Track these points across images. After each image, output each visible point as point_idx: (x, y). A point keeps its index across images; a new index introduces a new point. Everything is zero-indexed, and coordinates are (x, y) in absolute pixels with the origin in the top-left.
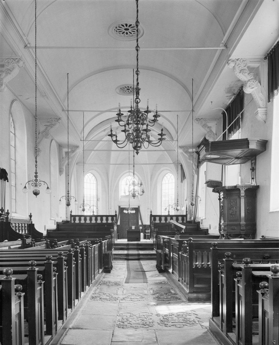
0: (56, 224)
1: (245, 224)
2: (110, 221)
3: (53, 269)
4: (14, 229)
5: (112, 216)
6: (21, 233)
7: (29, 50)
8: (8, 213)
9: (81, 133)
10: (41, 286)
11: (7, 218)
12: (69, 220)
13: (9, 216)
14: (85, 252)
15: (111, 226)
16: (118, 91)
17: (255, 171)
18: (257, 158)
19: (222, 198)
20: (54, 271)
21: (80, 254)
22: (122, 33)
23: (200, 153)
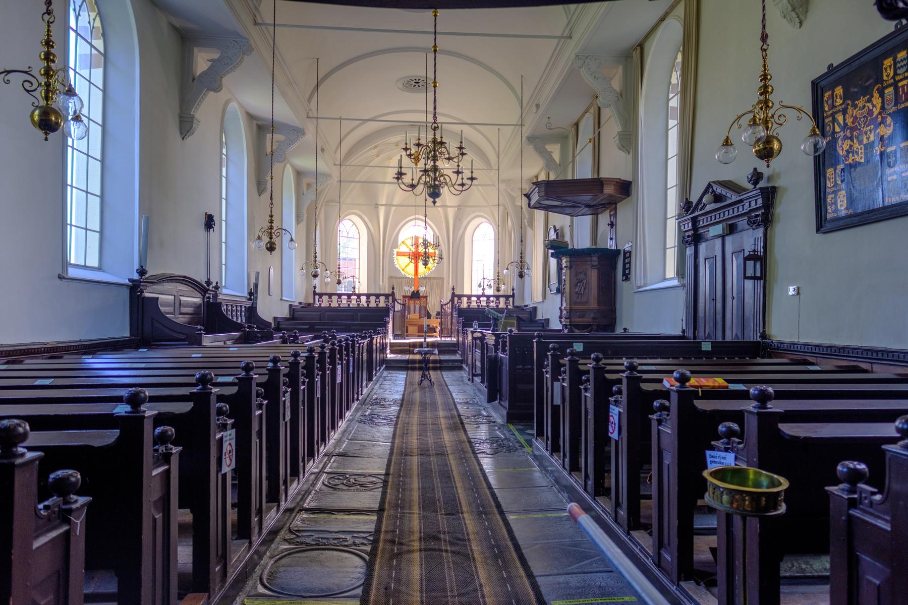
0: (886, 490)
2: (382, 304)
3: (283, 380)
5: (387, 296)
6: (239, 321)
8: (217, 288)
10: (262, 409)
12: (311, 301)
15: (386, 311)
16: (400, 86)
17: (614, 227)
20: (302, 375)
21: (328, 358)
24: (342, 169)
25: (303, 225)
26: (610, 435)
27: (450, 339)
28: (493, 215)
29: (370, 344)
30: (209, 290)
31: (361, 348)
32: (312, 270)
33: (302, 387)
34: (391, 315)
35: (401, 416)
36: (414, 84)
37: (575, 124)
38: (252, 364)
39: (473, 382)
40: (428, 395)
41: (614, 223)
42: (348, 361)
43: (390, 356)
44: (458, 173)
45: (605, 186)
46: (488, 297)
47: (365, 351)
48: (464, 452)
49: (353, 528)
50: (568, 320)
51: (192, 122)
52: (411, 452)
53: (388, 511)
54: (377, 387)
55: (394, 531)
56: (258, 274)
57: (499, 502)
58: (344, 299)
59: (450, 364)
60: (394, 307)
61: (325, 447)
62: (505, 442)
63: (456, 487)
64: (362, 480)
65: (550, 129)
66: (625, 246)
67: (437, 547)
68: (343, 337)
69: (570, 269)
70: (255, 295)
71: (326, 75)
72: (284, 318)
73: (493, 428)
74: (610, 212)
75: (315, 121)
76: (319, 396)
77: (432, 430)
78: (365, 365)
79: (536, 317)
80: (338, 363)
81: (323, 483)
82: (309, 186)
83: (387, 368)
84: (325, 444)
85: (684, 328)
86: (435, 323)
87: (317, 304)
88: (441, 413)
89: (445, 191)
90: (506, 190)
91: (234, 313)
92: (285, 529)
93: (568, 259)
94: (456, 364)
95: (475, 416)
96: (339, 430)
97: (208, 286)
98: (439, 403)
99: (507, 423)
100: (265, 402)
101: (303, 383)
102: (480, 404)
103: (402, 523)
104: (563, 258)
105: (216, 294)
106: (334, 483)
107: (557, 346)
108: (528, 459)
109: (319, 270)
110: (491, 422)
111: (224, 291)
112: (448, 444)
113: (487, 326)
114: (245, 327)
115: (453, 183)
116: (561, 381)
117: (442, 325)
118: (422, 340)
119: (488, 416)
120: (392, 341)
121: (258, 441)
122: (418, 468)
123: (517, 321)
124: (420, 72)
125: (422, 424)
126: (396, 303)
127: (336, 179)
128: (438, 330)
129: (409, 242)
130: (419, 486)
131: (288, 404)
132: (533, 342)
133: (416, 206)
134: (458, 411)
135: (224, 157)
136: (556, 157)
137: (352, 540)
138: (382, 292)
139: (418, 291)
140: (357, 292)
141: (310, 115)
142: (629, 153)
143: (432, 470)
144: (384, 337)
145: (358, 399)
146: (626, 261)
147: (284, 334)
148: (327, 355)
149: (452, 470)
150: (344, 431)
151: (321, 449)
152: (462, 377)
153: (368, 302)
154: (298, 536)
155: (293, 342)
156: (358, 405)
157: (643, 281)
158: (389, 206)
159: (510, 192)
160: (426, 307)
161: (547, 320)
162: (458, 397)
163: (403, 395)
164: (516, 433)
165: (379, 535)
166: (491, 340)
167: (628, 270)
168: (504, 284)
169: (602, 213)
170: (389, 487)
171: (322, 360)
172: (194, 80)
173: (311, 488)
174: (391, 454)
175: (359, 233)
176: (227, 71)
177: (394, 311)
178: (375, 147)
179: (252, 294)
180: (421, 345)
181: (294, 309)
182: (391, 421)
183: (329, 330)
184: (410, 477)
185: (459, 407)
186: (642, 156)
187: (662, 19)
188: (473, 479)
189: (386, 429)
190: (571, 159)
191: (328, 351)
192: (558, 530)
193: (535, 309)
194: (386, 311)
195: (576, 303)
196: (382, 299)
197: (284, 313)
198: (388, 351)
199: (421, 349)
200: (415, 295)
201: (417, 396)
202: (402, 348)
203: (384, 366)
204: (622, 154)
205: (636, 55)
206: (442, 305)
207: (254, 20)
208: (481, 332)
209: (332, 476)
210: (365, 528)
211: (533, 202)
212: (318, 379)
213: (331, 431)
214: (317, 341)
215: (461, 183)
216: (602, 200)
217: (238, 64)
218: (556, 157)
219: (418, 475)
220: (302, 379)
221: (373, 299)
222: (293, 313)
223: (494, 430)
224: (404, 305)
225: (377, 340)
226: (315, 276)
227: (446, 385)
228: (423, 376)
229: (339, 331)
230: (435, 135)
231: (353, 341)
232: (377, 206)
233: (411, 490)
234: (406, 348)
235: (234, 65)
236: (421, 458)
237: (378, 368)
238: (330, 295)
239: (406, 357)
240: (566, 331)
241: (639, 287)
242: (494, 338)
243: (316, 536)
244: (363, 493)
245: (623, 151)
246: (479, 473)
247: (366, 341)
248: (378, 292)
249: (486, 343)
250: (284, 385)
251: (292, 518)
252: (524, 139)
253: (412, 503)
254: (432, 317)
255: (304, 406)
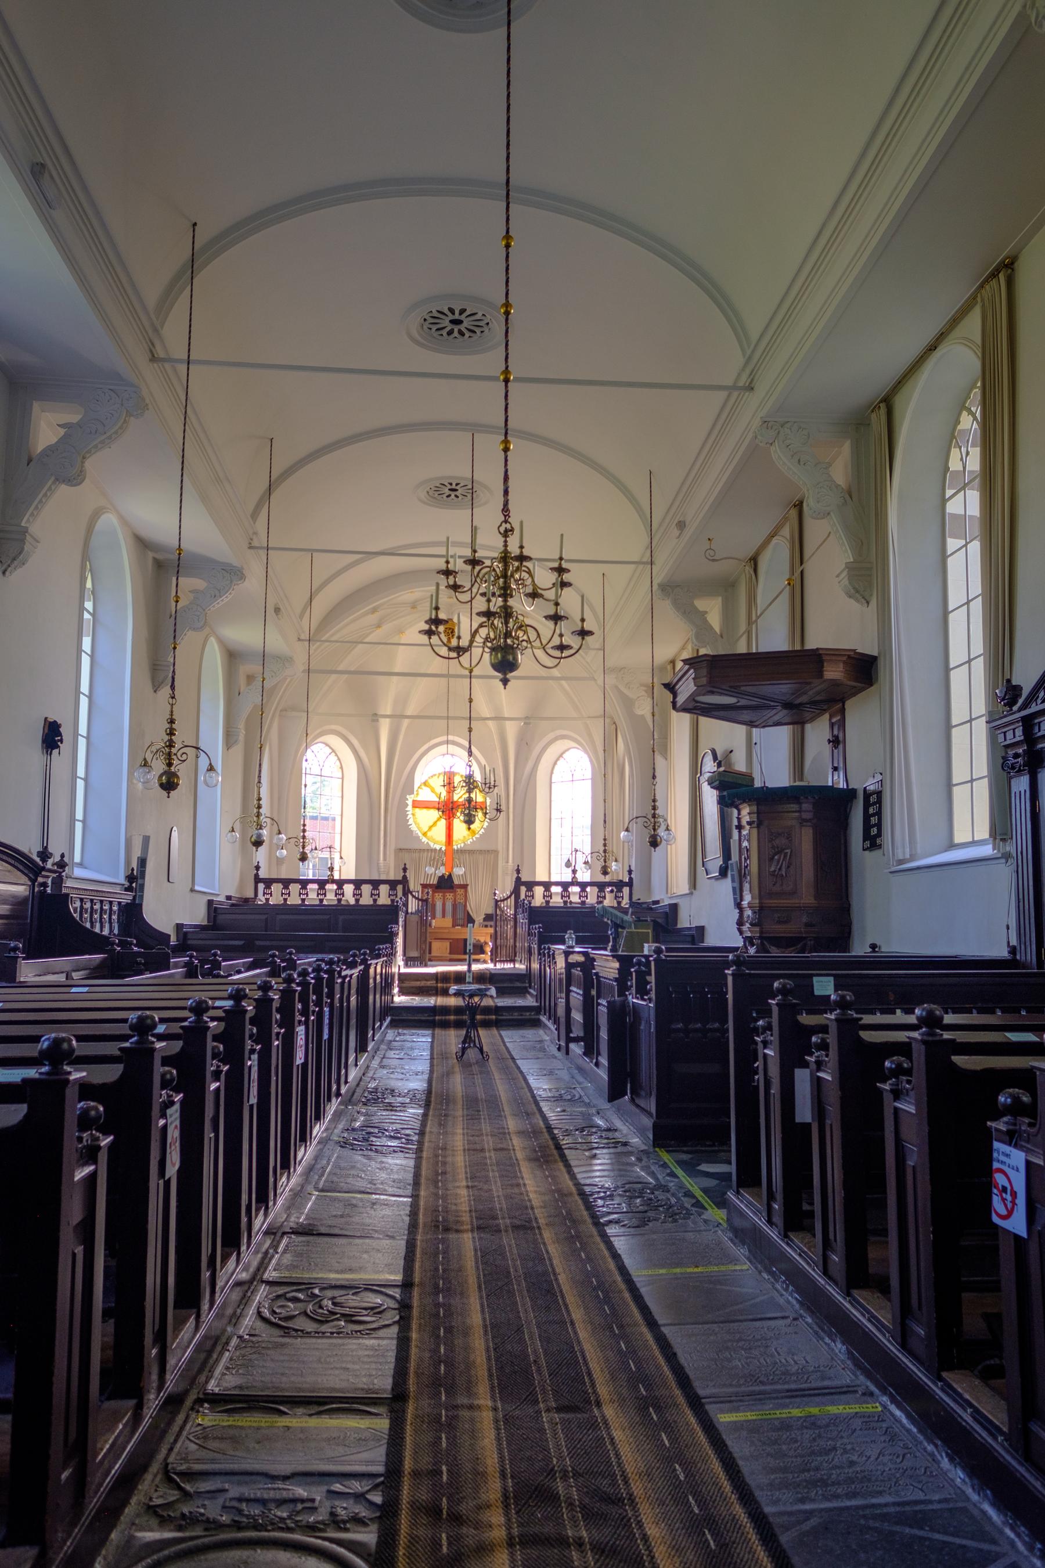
1: (817, 905)
2: (384, 899)
4: (76, 916)
5: (393, 884)
6: (106, 932)
7: (163, 367)
8: (62, 865)
9: (301, 616)
11: (58, 882)
12: (250, 894)
13: (64, 874)
14: (326, 990)
15: (392, 912)
16: (423, 495)
17: (841, 746)
18: (846, 707)
19: (748, 822)
20: (165, 1084)
22: (438, 330)
23: (677, 687)
24: (313, 648)
25: (238, 749)
26: (995, 1219)
27: (512, 966)
28: (590, 735)
29: (364, 977)
30: (44, 869)
31: (346, 985)
32: (253, 832)
33: (213, 1086)
34: (401, 923)
35: (428, 1129)
36: (448, 492)
37: (750, 559)
38: (70, 1041)
39: (567, 1053)
40: (478, 1080)
41: (841, 738)
42: (320, 1016)
43: (399, 999)
44: (556, 618)
45: (825, 664)
46: (583, 886)
47: (353, 991)
48: (574, 1221)
49: (330, 1460)
50: (757, 929)
51: (23, 541)
52: (458, 1222)
53: (417, 1399)
54: (375, 1063)
55: (437, 1473)
56: (146, 840)
57: (682, 1368)
58: (311, 889)
59: (516, 1016)
60: (406, 905)
61: (266, 1215)
62: (661, 1195)
63: (572, 1323)
64: (352, 1301)
65: (714, 560)
66: (866, 781)
67: (549, 1529)
68: (309, 964)
69: (758, 827)
70: (140, 881)
71: (286, 472)
72: (196, 926)
73: (625, 1159)
74: (831, 717)
75: (263, 553)
76: (254, 1100)
77: (498, 1164)
78: (353, 1022)
79: (676, 924)
80: (300, 1022)
81: (259, 1313)
82: (250, 678)
83: (394, 1024)
84: (267, 1208)
85: (1014, 942)
86: (482, 934)
87: (261, 899)
88: (512, 1124)
89: (523, 659)
90: (617, 687)
91: (96, 916)
92: (155, 1467)
93: (755, 808)
94: (527, 1015)
95: (582, 1130)
96: (299, 1169)
97: (44, 860)
98: (503, 1099)
99: (654, 1146)
100: (106, 1141)
101: (217, 1074)
102: (587, 1101)
103: (452, 1441)
104: (741, 807)
105: (60, 877)
106: (284, 1312)
107: (790, 984)
108: (719, 1243)
109: (265, 832)
110: (620, 1147)
111: (78, 872)
112: (536, 1200)
113: (600, 941)
114: (113, 943)
115: (544, 642)
116: (814, 1066)
117: (496, 939)
118: (464, 968)
119: (609, 1130)
120: (403, 970)
121: (79, 1250)
122: (477, 1268)
123: (654, 930)
124: (460, 471)
125: (474, 1150)
126: (410, 897)
127: (300, 665)
128: (488, 949)
129: (438, 783)
130: (484, 1319)
131: (174, 1134)
132: (726, 975)
133: (448, 718)
134: (544, 1118)
135: (86, 616)
136: (715, 620)
137: (328, 1504)
138: (383, 877)
139: (450, 876)
140: (336, 877)
141: (255, 543)
142: (868, 603)
143: (509, 1272)
144: (389, 963)
145: (338, 1094)
146: (871, 811)
147: (191, 956)
148: (276, 1005)
149: (555, 1274)
150: (310, 1169)
151: (257, 1223)
152: (541, 1041)
153: (358, 895)
154: (186, 1495)
155: (209, 974)
156: (340, 1104)
157: (908, 850)
158: (397, 717)
159: (626, 691)
160: (465, 906)
161: (701, 930)
162: (541, 1086)
163: (430, 1082)
164: (679, 1172)
165: (398, 1489)
166: (607, 966)
167: (875, 829)
168: (616, 861)
169: (812, 720)
170: (414, 1325)
171: (262, 1018)
172: (30, 461)
173: (229, 1329)
174: (413, 1226)
175: (342, 768)
176: (96, 446)
177: (407, 913)
178: (374, 610)
179: (135, 880)
180: (459, 978)
181: (216, 908)
182: (409, 1142)
183: (282, 949)
184: (462, 1294)
185: (545, 1107)
186: (897, 606)
187: (932, 348)
188: (607, 1299)
189: (398, 1162)
190: (743, 627)
191: (276, 997)
192: (852, 1463)
193: (674, 907)
194: (392, 912)
195: (771, 895)
196: (384, 889)
197: (196, 915)
198: (396, 990)
199: (463, 987)
200: (445, 884)
201: (457, 1083)
202: (423, 983)
203: (388, 1019)
204: (854, 606)
205: (878, 420)
206: (497, 901)
207: (151, 351)
208: (585, 954)
209: (281, 1290)
210: (361, 1462)
211: (681, 699)
212: (252, 1062)
213: (282, 1175)
214: (258, 971)
215: (558, 643)
216: (818, 693)
217: (116, 432)
218: (715, 620)
219: (480, 1287)
220: (212, 1065)
221: (366, 889)
222: (215, 917)
223: (628, 1164)
224: (425, 901)
225: (377, 967)
226: (258, 843)
227: (513, 1058)
228: (467, 1039)
229: (299, 950)
230: (506, 546)
231: (331, 972)
232: (375, 717)
233: (466, 1332)
234: (429, 983)
235: (108, 434)
236: (480, 1239)
237: (378, 1024)
238: (286, 883)
239: (430, 1001)
240: (752, 951)
241: (901, 862)
242: (617, 965)
243: (234, 1491)
244: (352, 1344)
245: (857, 600)
246: (619, 1279)
247: (355, 972)
248: (375, 877)
249: (597, 974)
250: (163, 1088)
251: (175, 1428)
252: (655, 587)
253: (473, 1373)
254: (476, 923)
255: (216, 1130)
